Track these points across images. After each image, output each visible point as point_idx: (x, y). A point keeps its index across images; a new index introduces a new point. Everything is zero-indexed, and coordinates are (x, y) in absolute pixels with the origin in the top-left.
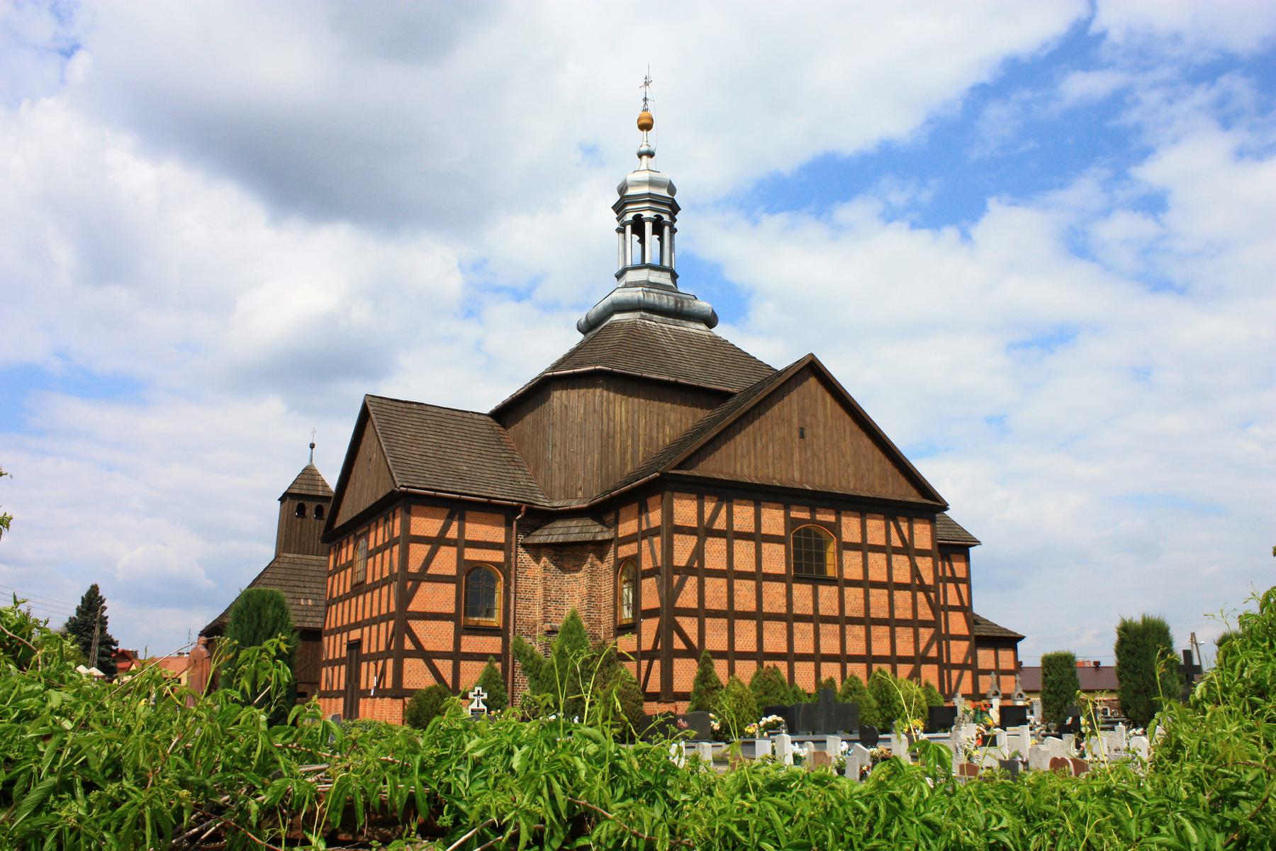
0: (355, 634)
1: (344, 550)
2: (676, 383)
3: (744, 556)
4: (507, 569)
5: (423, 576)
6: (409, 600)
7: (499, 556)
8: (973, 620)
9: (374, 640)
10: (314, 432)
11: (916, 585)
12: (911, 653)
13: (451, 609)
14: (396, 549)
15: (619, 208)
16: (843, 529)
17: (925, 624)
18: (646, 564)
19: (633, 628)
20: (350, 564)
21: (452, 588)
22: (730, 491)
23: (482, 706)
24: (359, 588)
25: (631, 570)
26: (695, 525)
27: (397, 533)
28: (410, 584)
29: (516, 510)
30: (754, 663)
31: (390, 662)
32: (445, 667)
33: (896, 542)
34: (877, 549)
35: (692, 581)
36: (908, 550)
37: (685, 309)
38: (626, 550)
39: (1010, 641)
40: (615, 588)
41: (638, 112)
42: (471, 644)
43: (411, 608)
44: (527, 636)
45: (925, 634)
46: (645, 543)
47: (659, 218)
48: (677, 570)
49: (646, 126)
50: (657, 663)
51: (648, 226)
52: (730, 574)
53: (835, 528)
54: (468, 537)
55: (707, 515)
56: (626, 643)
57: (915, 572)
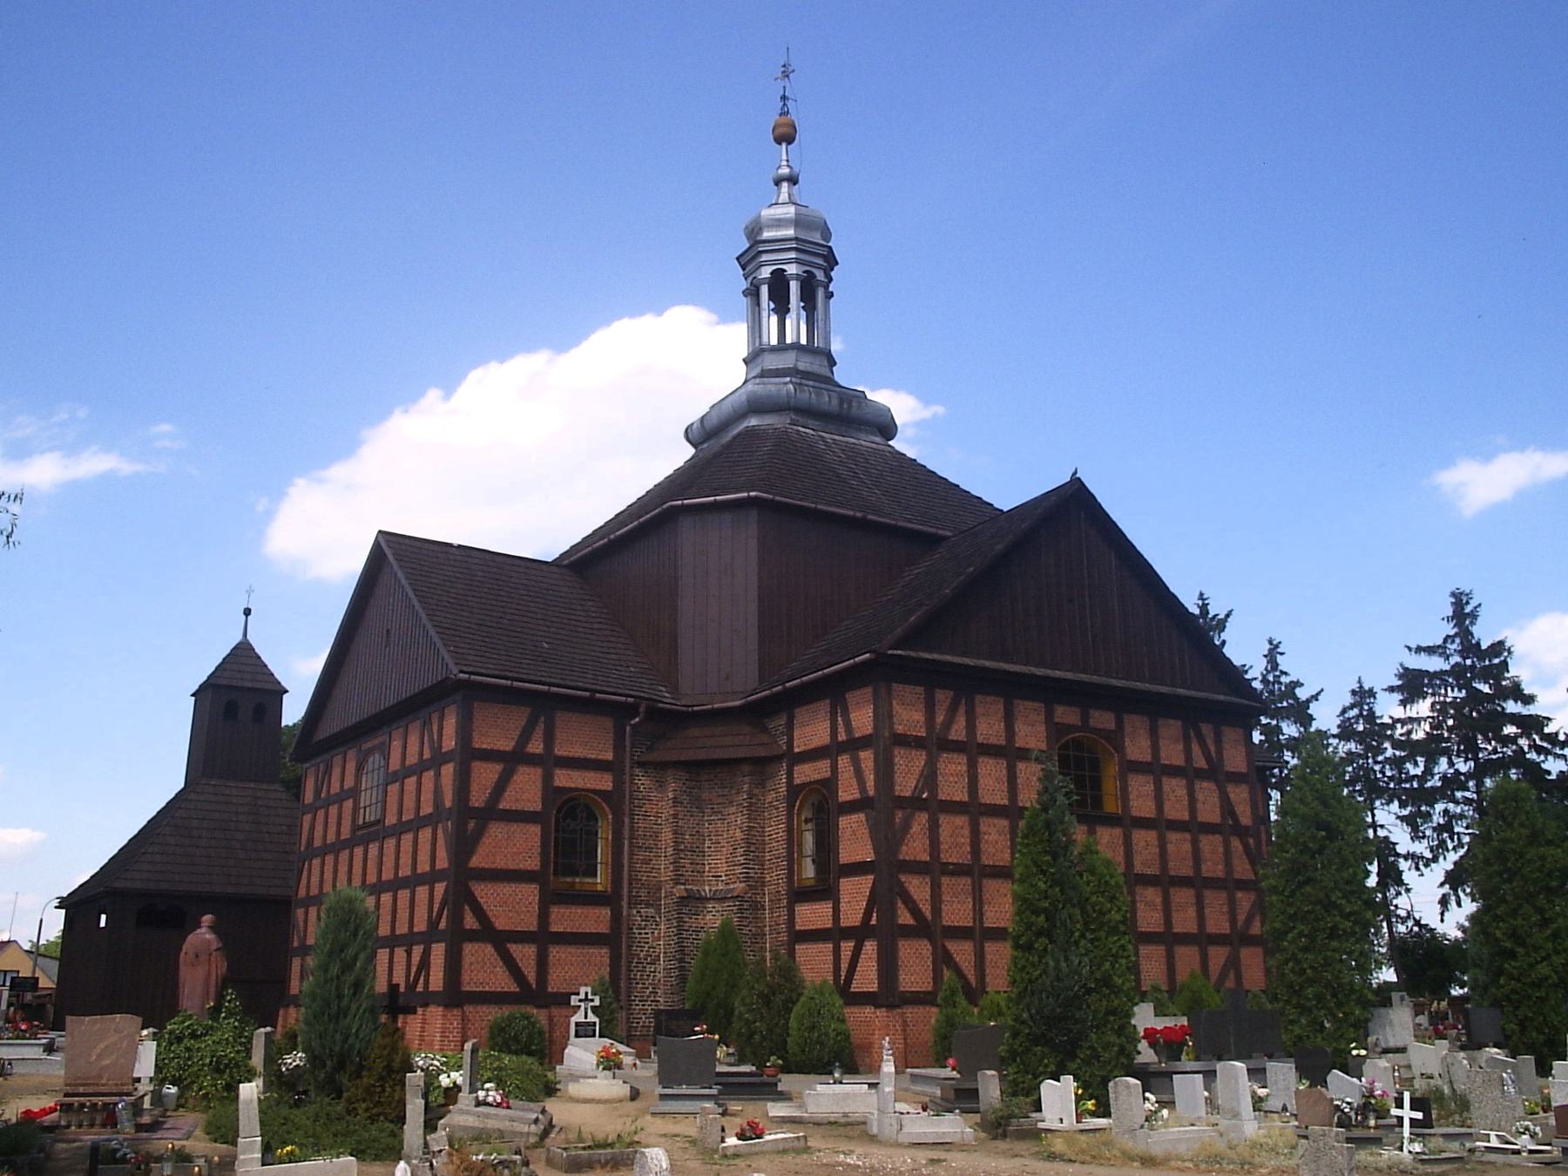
2: (864, 519)
5: (492, 813)
6: (471, 853)
7: (605, 782)
10: (249, 592)
12: (1225, 928)
13: (532, 863)
14: (448, 770)
15: (747, 261)
17: (1242, 885)
18: (847, 792)
19: (824, 890)
21: (535, 830)
22: (969, 685)
23: (592, 1018)
25: (822, 806)
27: (449, 743)
28: (471, 825)
29: (632, 710)
30: (469, 948)
31: (438, 951)
32: (525, 955)
33: (1200, 763)
34: (1174, 771)
35: (921, 820)
37: (854, 411)
38: (807, 773)
40: (790, 830)
41: (773, 117)
42: (565, 919)
43: (476, 861)
44: (648, 905)
45: (1245, 900)
46: (844, 761)
47: (810, 275)
48: (901, 802)
49: (785, 136)
50: (870, 947)
52: (974, 809)
53: (1115, 739)
54: (559, 751)
56: (814, 915)
57: (1228, 808)
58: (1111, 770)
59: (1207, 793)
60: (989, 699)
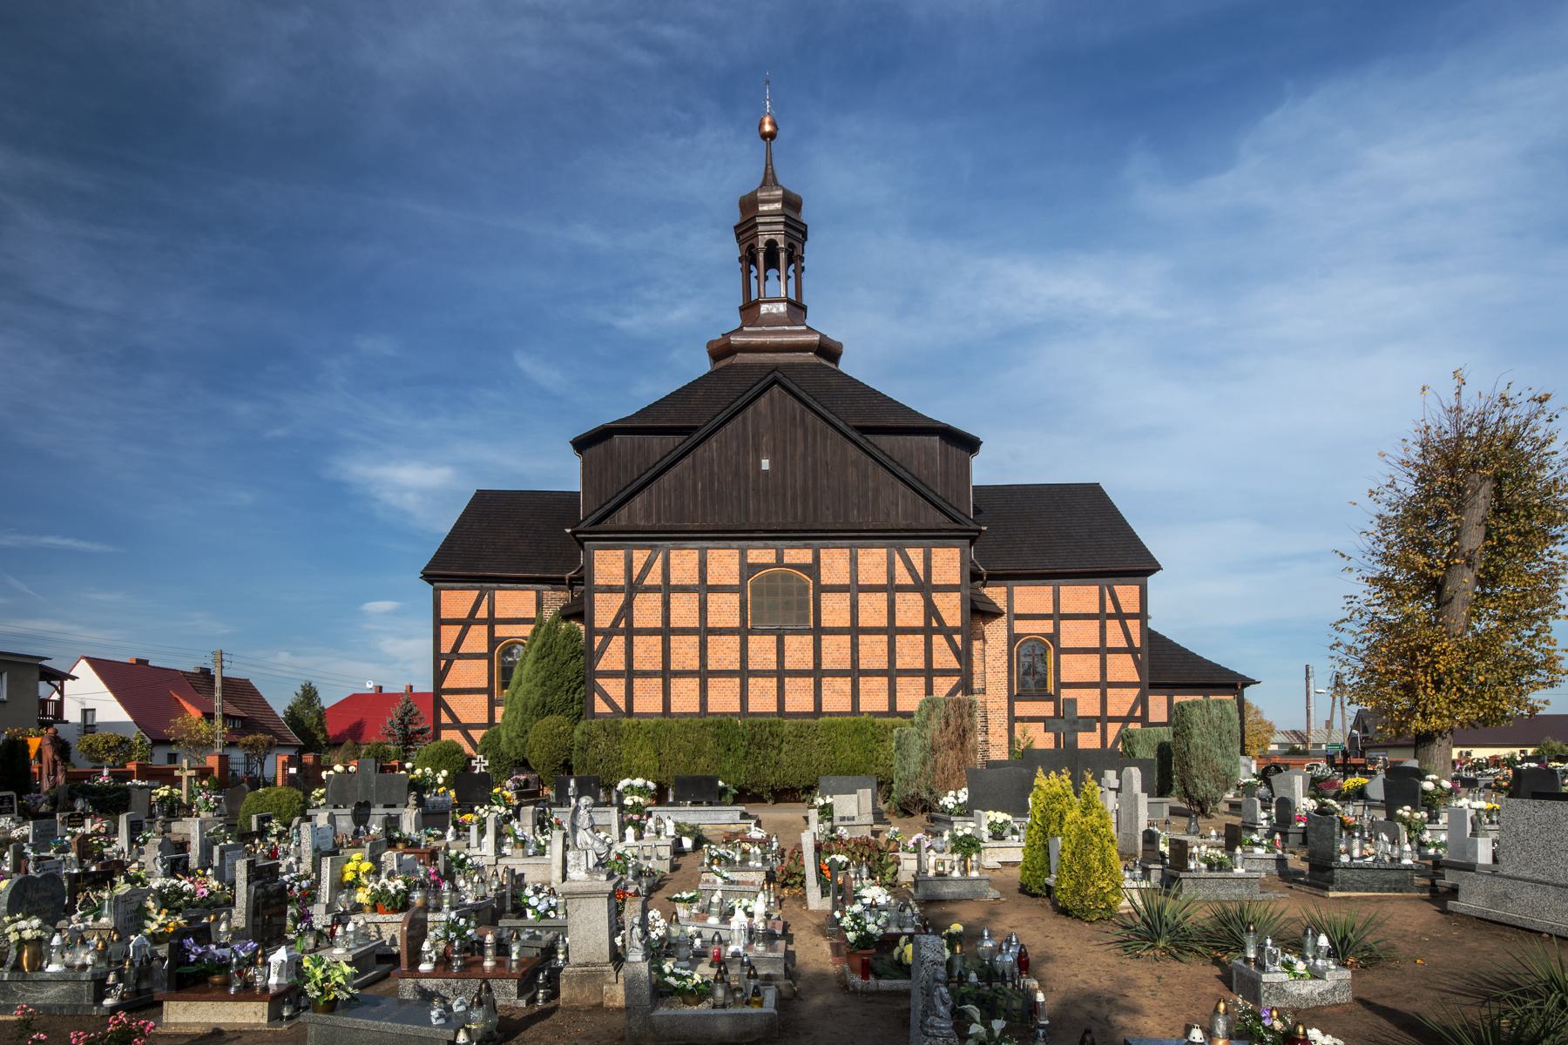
21: (735, 707)
33: (903, 577)
35: (618, 642)
36: (924, 586)
53: (813, 569)
55: (657, 566)
57: (931, 610)
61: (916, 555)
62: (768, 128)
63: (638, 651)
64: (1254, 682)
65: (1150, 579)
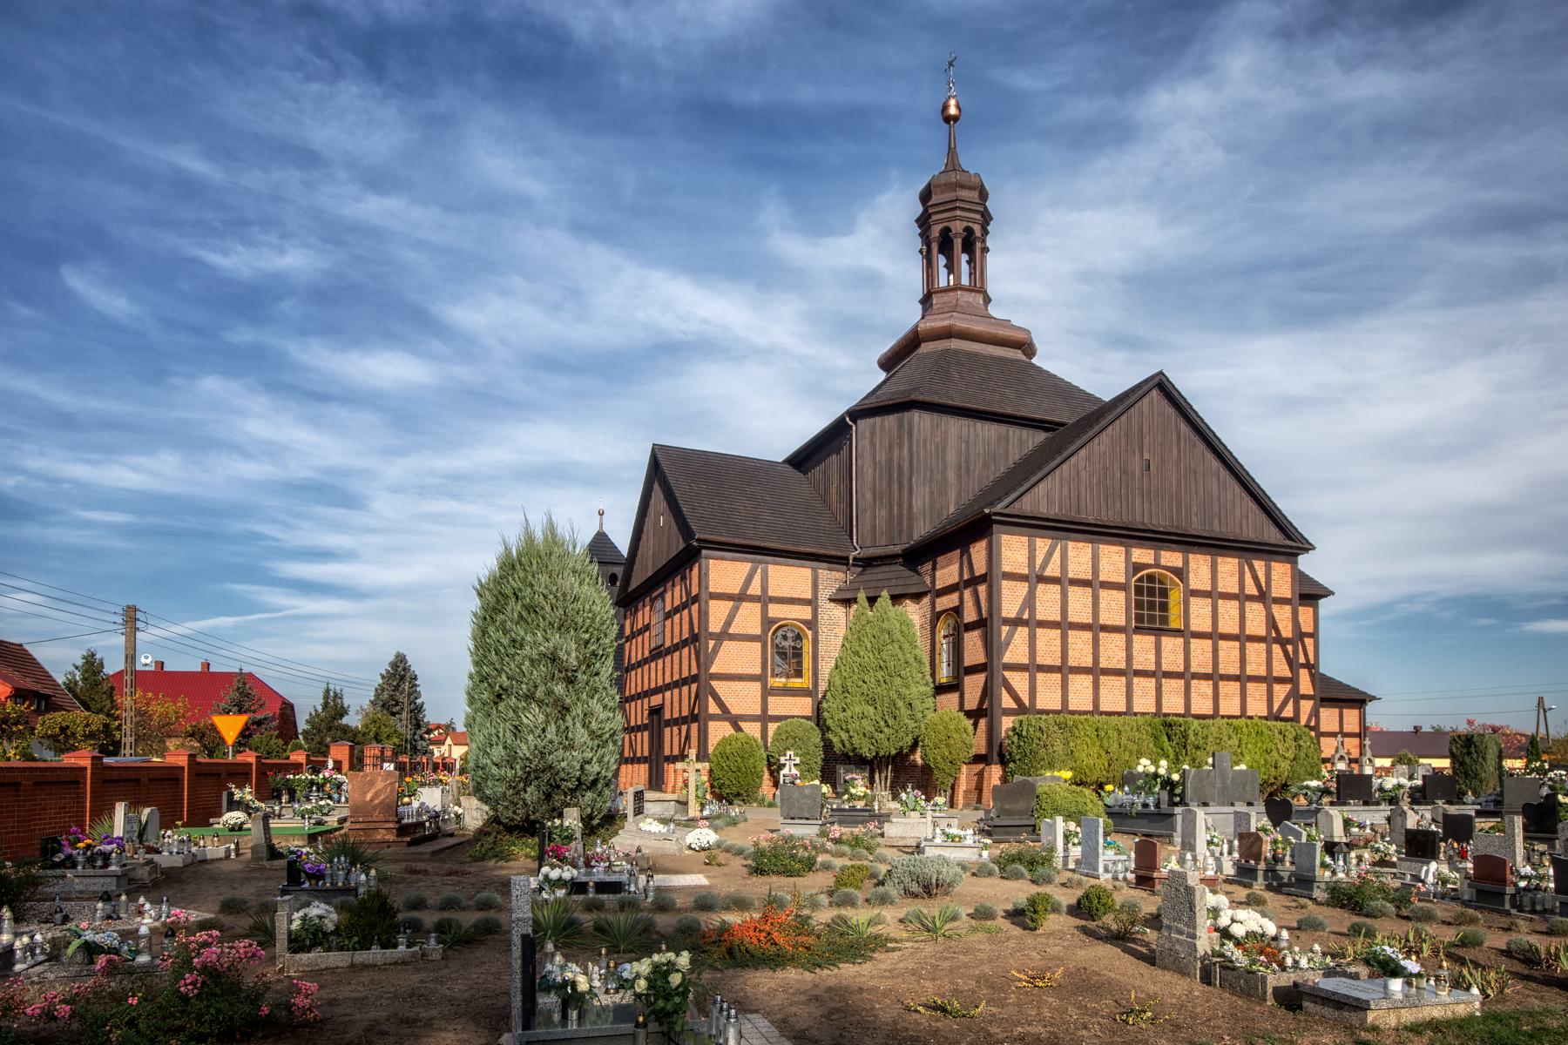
0: (656, 700)
1: (640, 614)
3: (1080, 605)
4: (812, 624)
8: (1318, 679)
9: (676, 705)
11: (1273, 637)
15: (924, 222)
16: (1191, 575)
18: (970, 615)
19: (954, 687)
20: (647, 628)
21: (1006, 568)
24: (658, 653)
26: (1026, 571)
33: (1251, 589)
36: (1263, 596)
39: (1359, 701)
45: (1281, 691)
47: (969, 230)
51: (958, 243)
53: (1181, 573)
57: (1272, 623)
58: (1175, 597)
59: (1255, 612)
60: (1081, 545)
61: (1259, 565)
62: (953, 111)
63: (1040, 644)
64: (1373, 698)
65: (1321, 602)
